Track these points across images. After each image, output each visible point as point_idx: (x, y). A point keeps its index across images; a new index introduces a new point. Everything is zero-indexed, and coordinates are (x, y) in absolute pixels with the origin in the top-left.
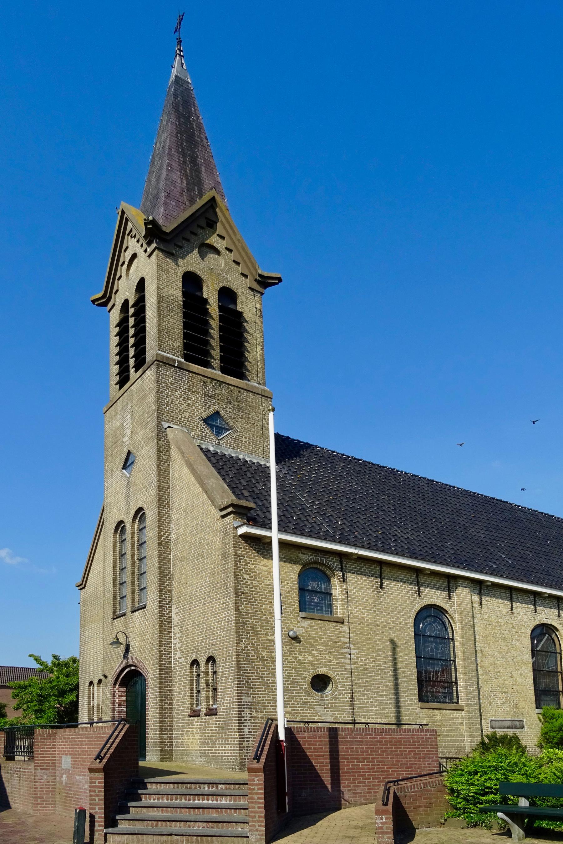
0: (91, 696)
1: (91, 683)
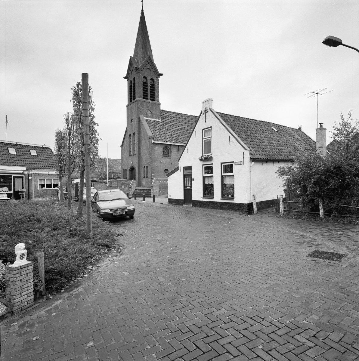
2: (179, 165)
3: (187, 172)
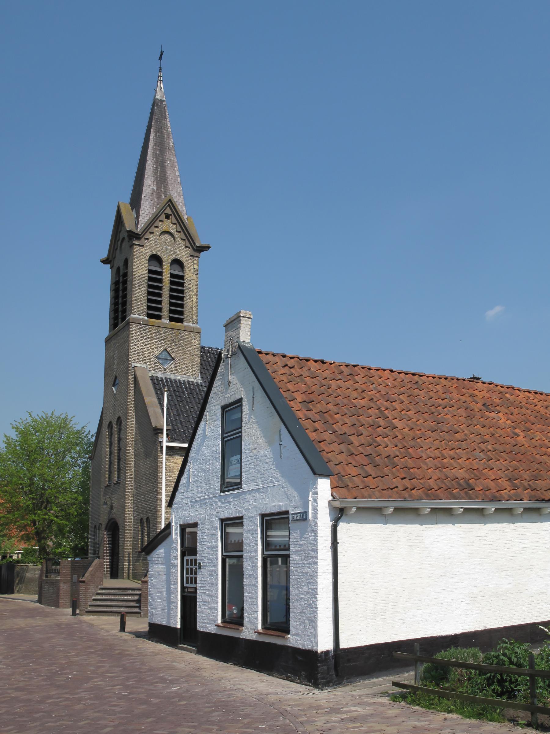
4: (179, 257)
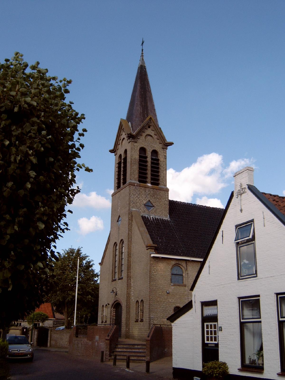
0: (103, 311)
1: (103, 306)
2: (193, 296)
3: (209, 311)
4: (156, 149)
